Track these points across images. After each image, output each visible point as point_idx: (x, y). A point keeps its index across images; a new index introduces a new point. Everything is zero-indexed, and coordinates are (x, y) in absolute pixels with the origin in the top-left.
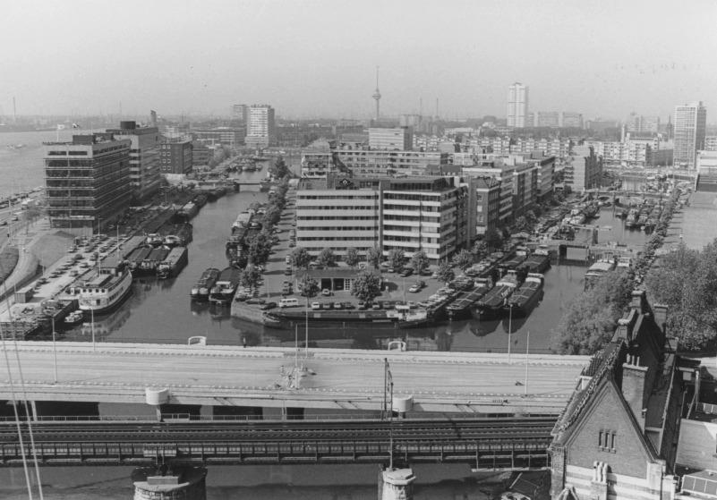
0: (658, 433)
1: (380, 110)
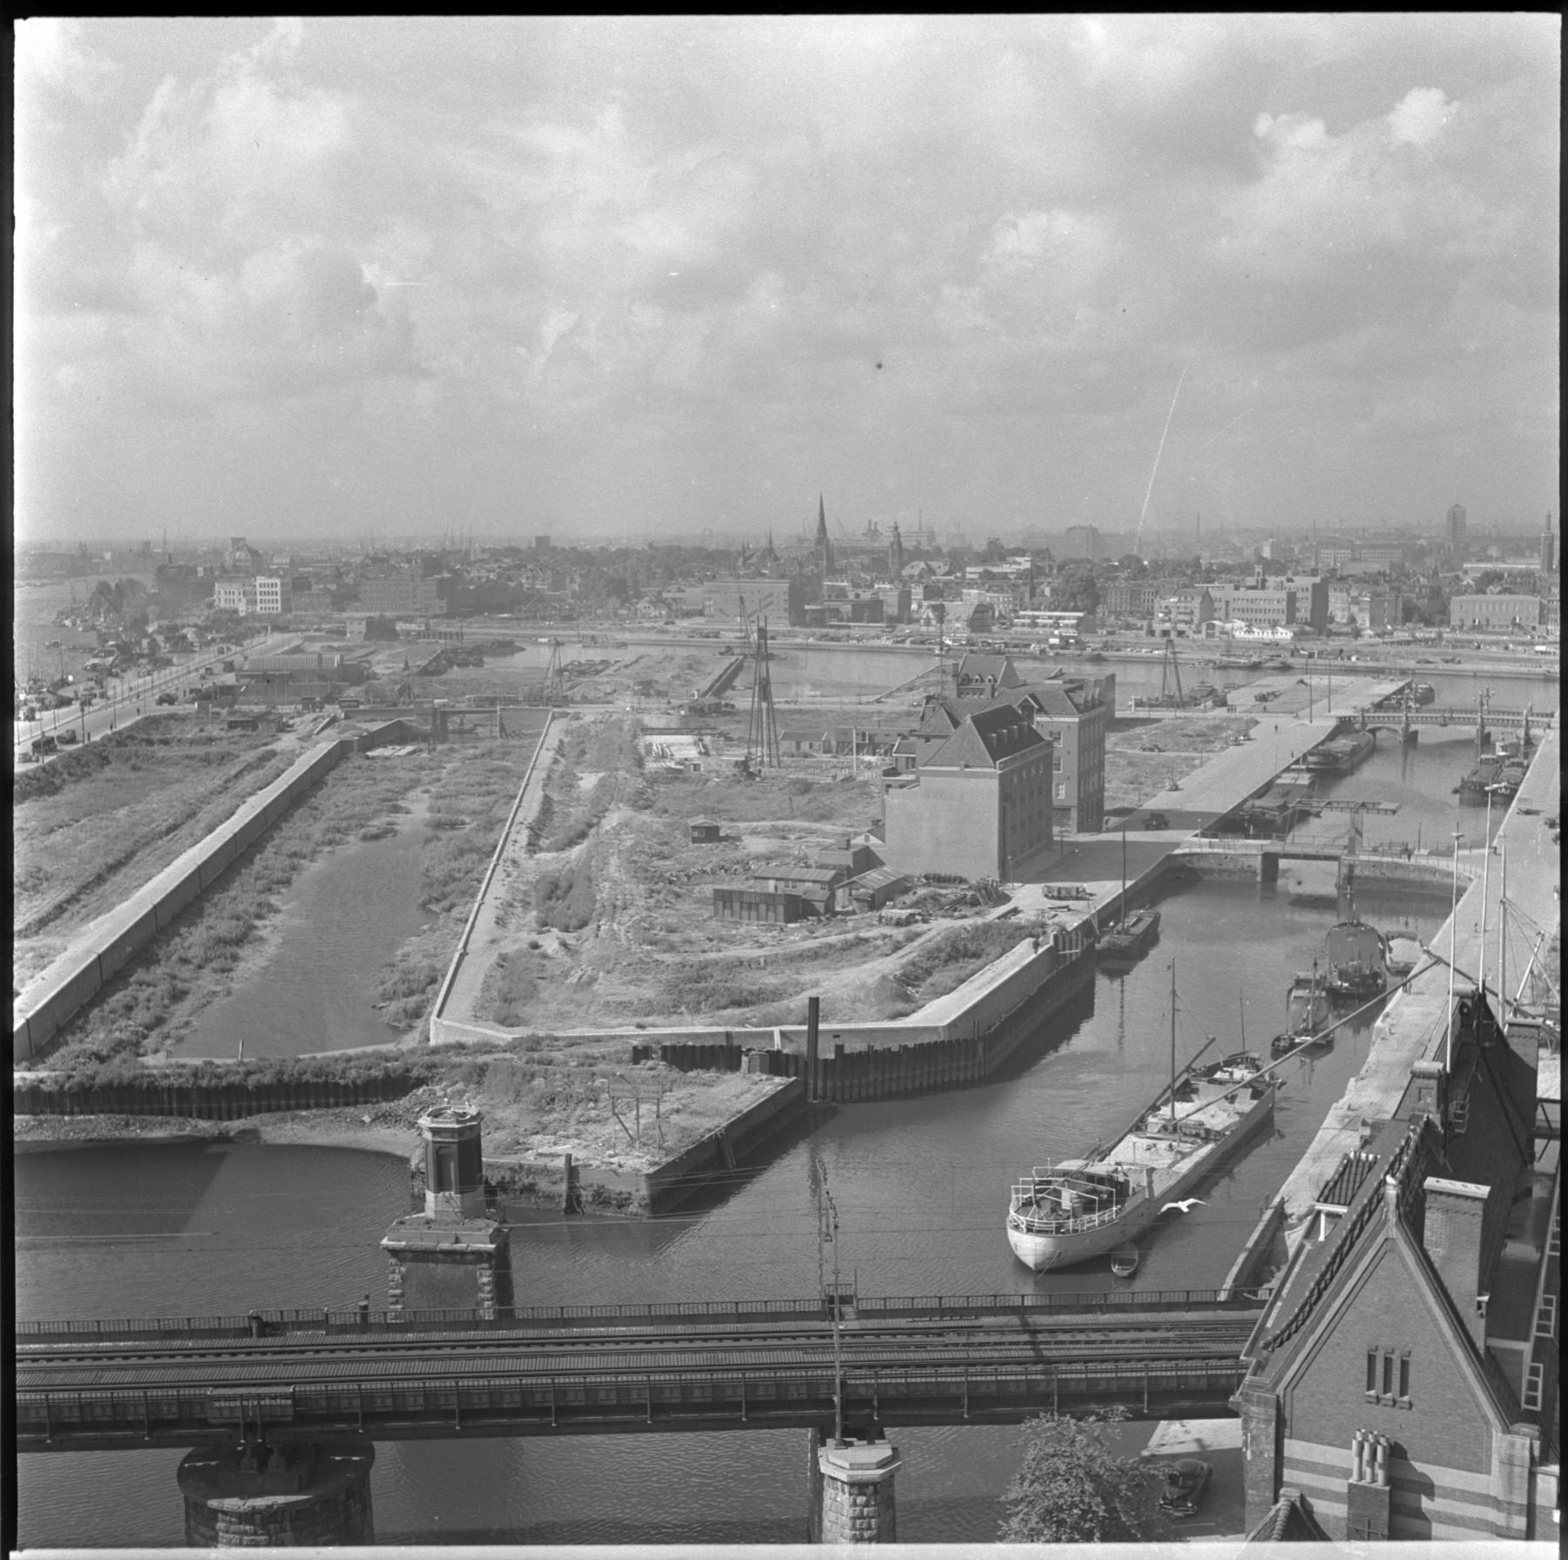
0: (1521, 1352)
1: (674, 725)
